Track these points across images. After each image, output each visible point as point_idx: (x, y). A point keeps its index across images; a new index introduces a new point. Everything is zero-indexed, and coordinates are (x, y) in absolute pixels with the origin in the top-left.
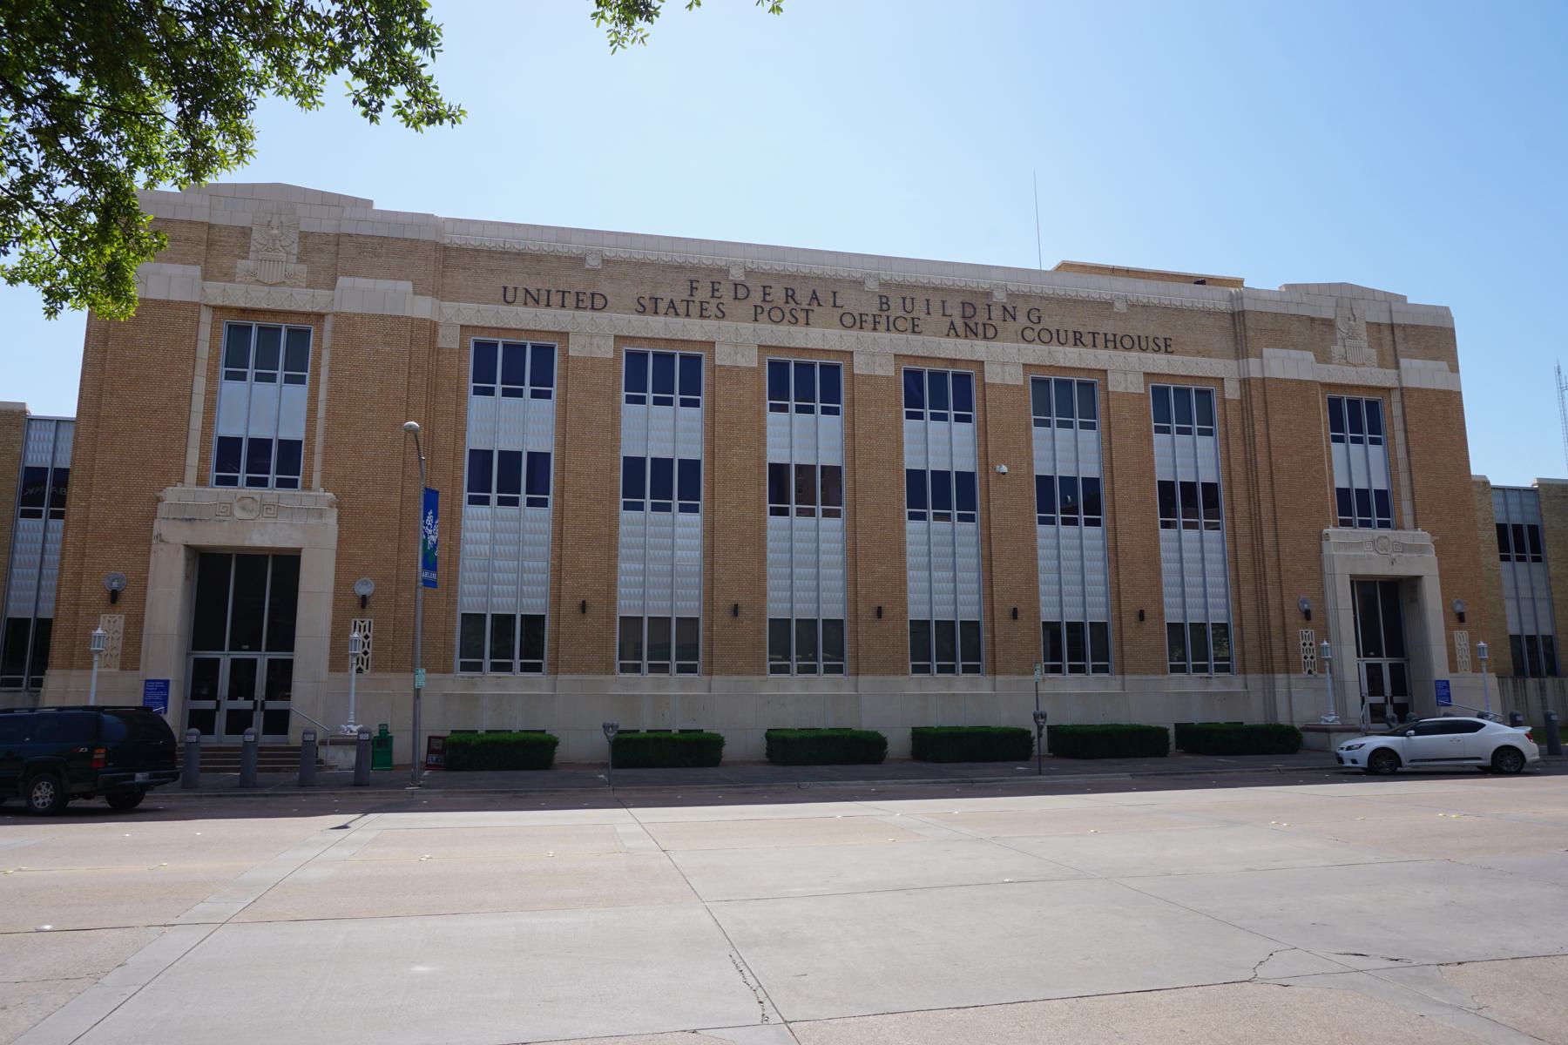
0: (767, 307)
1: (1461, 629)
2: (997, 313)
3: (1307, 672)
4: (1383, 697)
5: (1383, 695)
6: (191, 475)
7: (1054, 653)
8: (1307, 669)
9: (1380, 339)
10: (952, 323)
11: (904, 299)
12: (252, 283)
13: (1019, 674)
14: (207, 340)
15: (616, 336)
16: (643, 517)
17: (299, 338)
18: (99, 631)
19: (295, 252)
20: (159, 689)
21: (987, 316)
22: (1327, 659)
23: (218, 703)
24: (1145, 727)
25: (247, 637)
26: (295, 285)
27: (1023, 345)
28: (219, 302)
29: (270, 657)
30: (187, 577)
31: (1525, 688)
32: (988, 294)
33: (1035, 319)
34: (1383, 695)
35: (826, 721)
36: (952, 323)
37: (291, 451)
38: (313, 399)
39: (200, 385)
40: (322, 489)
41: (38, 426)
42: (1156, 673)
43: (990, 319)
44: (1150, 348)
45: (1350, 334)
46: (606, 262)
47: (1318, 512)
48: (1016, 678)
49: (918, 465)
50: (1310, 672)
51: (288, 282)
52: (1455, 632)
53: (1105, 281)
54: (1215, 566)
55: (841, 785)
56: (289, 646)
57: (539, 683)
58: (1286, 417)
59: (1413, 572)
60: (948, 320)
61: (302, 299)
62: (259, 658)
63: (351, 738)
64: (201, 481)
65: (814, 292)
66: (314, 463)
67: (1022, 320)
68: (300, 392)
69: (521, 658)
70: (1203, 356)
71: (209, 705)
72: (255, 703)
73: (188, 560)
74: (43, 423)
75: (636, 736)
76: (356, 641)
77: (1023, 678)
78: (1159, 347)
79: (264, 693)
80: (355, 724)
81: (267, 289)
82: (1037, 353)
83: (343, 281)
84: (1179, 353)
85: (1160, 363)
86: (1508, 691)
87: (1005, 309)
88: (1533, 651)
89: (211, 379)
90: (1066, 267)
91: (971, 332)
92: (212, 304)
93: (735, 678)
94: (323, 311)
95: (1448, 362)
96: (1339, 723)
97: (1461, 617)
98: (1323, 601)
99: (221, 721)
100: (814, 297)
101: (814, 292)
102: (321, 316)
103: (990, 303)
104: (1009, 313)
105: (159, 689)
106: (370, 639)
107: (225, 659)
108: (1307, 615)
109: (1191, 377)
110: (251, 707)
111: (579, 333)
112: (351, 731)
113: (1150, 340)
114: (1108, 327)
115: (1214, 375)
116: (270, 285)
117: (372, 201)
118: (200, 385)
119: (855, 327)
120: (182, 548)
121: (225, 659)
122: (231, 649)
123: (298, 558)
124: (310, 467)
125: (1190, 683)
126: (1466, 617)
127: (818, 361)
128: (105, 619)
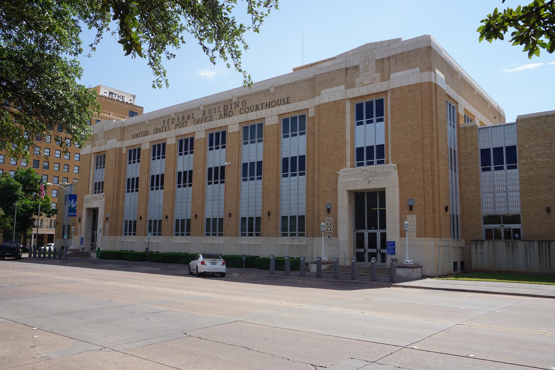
0: (178, 124)
1: (412, 214)
2: (233, 106)
3: (327, 237)
4: (376, 249)
5: (376, 248)
6: (348, 163)
7: (284, 229)
8: (328, 235)
9: (383, 67)
10: (221, 114)
11: (209, 110)
12: (361, 86)
13: (231, 236)
14: (349, 111)
15: (150, 142)
16: (297, 178)
17: (380, 104)
18: (406, 222)
19: (375, 69)
20: (392, 245)
21: (230, 108)
22: (322, 231)
23: (365, 250)
24: (142, 252)
25: (372, 225)
26: (376, 82)
27: (241, 115)
28: (351, 97)
29: (369, 232)
30: (350, 202)
31: (549, 248)
32: (231, 100)
33: (244, 104)
34: (376, 248)
35: (252, 253)
36: (221, 114)
37: (381, 149)
38: (386, 127)
39: (348, 130)
40: (392, 163)
41: (487, 130)
42: (274, 237)
43: (231, 109)
44: (282, 104)
45: (366, 70)
46: (276, 88)
47: (339, 162)
48: (230, 238)
49: (285, 156)
50: (329, 237)
51: (373, 82)
52: (408, 216)
53: (311, 69)
54: (303, 191)
55: (142, 268)
56: (385, 228)
57: (304, 241)
58: (327, 120)
59: (379, 186)
60: (220, 113)
61: (379, 87)
62: (365, 232)
63: (407, 265)
64: (92, 194)
65: (188, 115)
66: (389, 153)
67: (241, 106)
68: (382, 124)
69: (248, 231)
70: (302, 101)
71: (362, 250)
72: (377, 250)
73: (350, 197)
74: (508, 126)
75: (187, 254)
76: (406, 224)
77: (232, 238)
78: (285, 102)
79: (380, 246)
80: (409, 259)
81: (366, 87)
82: (243, 118)
83: (392, 75)
84: (293, 102)
85: (284, 109)
86: (543, 250)
87: (236, 104)
88: (251, 229)
89: (94, 170)
90: (295, 70)
91: (226, 115)
92: (349, 98)
93: (166, 237)
94: (386, 90)
95: (322, 90)
96: (327, 260)
97: (411, 208)
98: (336, 204)
99: (366, 256)
100: (188, 117)
101: (188, 115)
102: (386, 92)
103: (232, 103)
104: (237, 105)
105: (392, 245)
106: (332, 225)
107: (366, 232)
108: (329, 210)
109: (259, 119)
110: (376, 252)
111: (267, 117)
112: (407, 262)
113: (282, 100)
114: (267, 100)
115: (304, 108)
116: (368, 85)
117: (401, 38)
118: (348, 130)
119: (276, 106)
120: (346, 191)
121: (366, 232)
122: (368, 229)
123: (385, 192)
124: (388, 156)
125: (287, 241)
126: (408, 208)
127: (374, 99)
128: (409, 217)
